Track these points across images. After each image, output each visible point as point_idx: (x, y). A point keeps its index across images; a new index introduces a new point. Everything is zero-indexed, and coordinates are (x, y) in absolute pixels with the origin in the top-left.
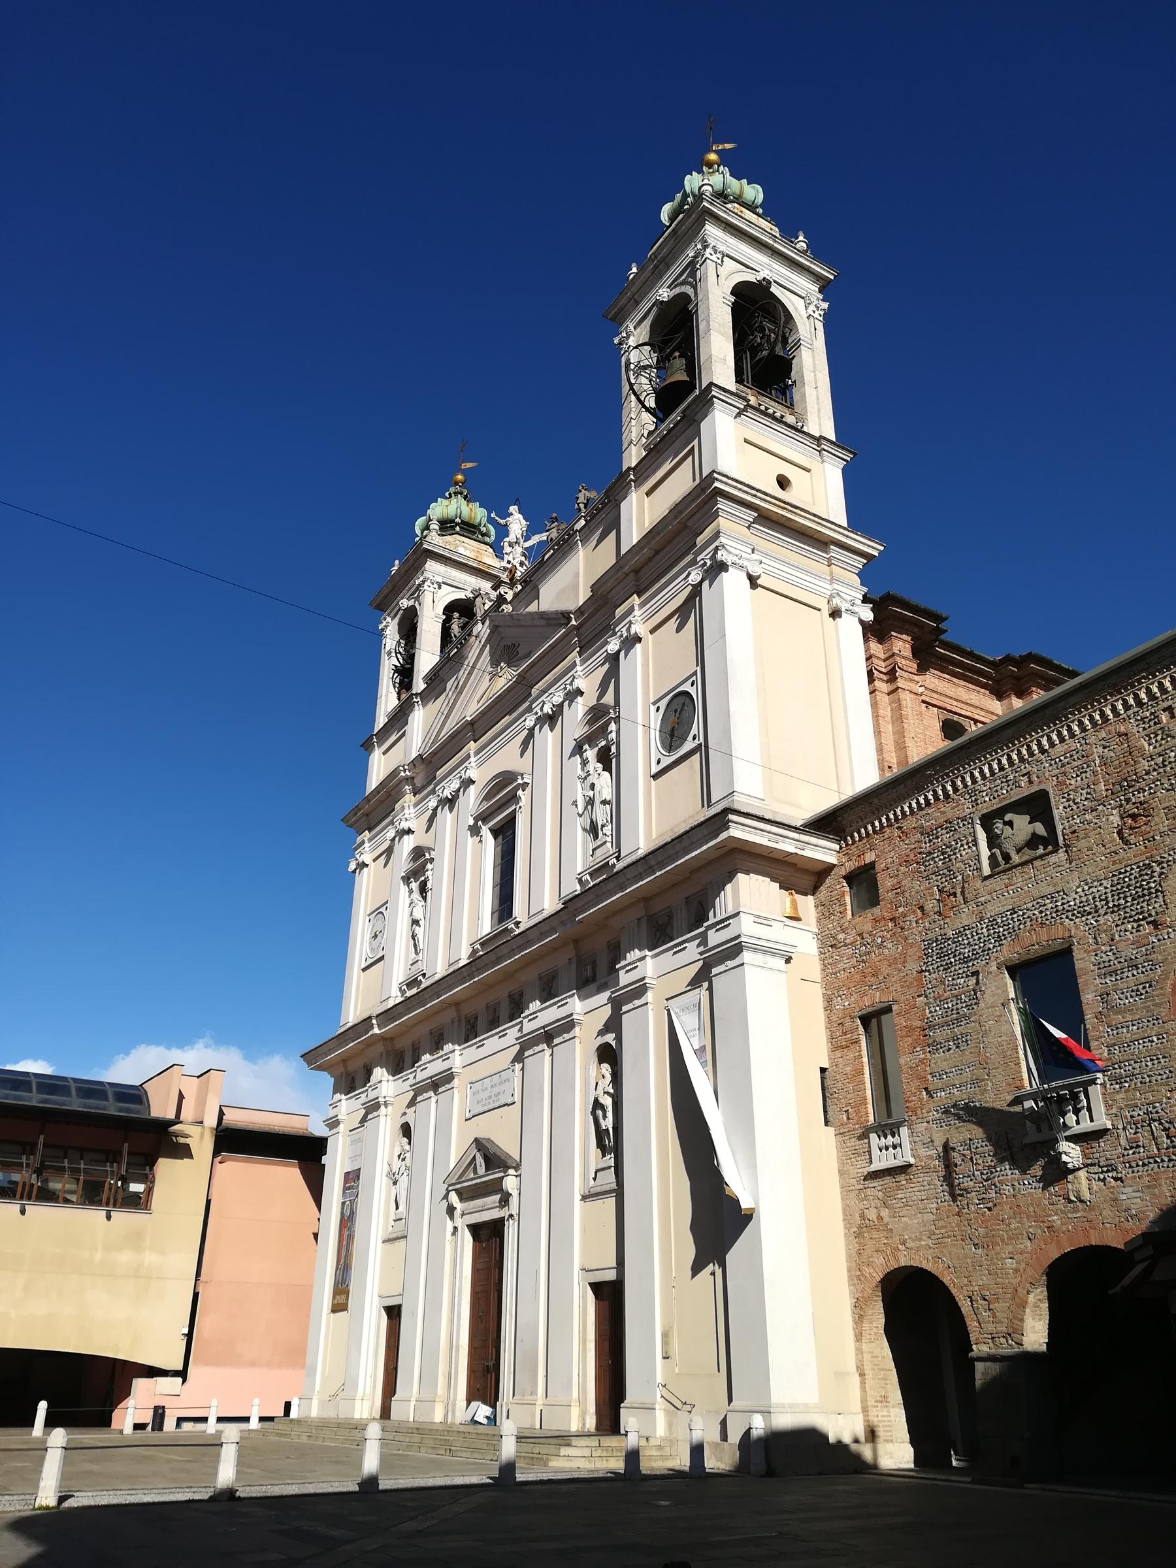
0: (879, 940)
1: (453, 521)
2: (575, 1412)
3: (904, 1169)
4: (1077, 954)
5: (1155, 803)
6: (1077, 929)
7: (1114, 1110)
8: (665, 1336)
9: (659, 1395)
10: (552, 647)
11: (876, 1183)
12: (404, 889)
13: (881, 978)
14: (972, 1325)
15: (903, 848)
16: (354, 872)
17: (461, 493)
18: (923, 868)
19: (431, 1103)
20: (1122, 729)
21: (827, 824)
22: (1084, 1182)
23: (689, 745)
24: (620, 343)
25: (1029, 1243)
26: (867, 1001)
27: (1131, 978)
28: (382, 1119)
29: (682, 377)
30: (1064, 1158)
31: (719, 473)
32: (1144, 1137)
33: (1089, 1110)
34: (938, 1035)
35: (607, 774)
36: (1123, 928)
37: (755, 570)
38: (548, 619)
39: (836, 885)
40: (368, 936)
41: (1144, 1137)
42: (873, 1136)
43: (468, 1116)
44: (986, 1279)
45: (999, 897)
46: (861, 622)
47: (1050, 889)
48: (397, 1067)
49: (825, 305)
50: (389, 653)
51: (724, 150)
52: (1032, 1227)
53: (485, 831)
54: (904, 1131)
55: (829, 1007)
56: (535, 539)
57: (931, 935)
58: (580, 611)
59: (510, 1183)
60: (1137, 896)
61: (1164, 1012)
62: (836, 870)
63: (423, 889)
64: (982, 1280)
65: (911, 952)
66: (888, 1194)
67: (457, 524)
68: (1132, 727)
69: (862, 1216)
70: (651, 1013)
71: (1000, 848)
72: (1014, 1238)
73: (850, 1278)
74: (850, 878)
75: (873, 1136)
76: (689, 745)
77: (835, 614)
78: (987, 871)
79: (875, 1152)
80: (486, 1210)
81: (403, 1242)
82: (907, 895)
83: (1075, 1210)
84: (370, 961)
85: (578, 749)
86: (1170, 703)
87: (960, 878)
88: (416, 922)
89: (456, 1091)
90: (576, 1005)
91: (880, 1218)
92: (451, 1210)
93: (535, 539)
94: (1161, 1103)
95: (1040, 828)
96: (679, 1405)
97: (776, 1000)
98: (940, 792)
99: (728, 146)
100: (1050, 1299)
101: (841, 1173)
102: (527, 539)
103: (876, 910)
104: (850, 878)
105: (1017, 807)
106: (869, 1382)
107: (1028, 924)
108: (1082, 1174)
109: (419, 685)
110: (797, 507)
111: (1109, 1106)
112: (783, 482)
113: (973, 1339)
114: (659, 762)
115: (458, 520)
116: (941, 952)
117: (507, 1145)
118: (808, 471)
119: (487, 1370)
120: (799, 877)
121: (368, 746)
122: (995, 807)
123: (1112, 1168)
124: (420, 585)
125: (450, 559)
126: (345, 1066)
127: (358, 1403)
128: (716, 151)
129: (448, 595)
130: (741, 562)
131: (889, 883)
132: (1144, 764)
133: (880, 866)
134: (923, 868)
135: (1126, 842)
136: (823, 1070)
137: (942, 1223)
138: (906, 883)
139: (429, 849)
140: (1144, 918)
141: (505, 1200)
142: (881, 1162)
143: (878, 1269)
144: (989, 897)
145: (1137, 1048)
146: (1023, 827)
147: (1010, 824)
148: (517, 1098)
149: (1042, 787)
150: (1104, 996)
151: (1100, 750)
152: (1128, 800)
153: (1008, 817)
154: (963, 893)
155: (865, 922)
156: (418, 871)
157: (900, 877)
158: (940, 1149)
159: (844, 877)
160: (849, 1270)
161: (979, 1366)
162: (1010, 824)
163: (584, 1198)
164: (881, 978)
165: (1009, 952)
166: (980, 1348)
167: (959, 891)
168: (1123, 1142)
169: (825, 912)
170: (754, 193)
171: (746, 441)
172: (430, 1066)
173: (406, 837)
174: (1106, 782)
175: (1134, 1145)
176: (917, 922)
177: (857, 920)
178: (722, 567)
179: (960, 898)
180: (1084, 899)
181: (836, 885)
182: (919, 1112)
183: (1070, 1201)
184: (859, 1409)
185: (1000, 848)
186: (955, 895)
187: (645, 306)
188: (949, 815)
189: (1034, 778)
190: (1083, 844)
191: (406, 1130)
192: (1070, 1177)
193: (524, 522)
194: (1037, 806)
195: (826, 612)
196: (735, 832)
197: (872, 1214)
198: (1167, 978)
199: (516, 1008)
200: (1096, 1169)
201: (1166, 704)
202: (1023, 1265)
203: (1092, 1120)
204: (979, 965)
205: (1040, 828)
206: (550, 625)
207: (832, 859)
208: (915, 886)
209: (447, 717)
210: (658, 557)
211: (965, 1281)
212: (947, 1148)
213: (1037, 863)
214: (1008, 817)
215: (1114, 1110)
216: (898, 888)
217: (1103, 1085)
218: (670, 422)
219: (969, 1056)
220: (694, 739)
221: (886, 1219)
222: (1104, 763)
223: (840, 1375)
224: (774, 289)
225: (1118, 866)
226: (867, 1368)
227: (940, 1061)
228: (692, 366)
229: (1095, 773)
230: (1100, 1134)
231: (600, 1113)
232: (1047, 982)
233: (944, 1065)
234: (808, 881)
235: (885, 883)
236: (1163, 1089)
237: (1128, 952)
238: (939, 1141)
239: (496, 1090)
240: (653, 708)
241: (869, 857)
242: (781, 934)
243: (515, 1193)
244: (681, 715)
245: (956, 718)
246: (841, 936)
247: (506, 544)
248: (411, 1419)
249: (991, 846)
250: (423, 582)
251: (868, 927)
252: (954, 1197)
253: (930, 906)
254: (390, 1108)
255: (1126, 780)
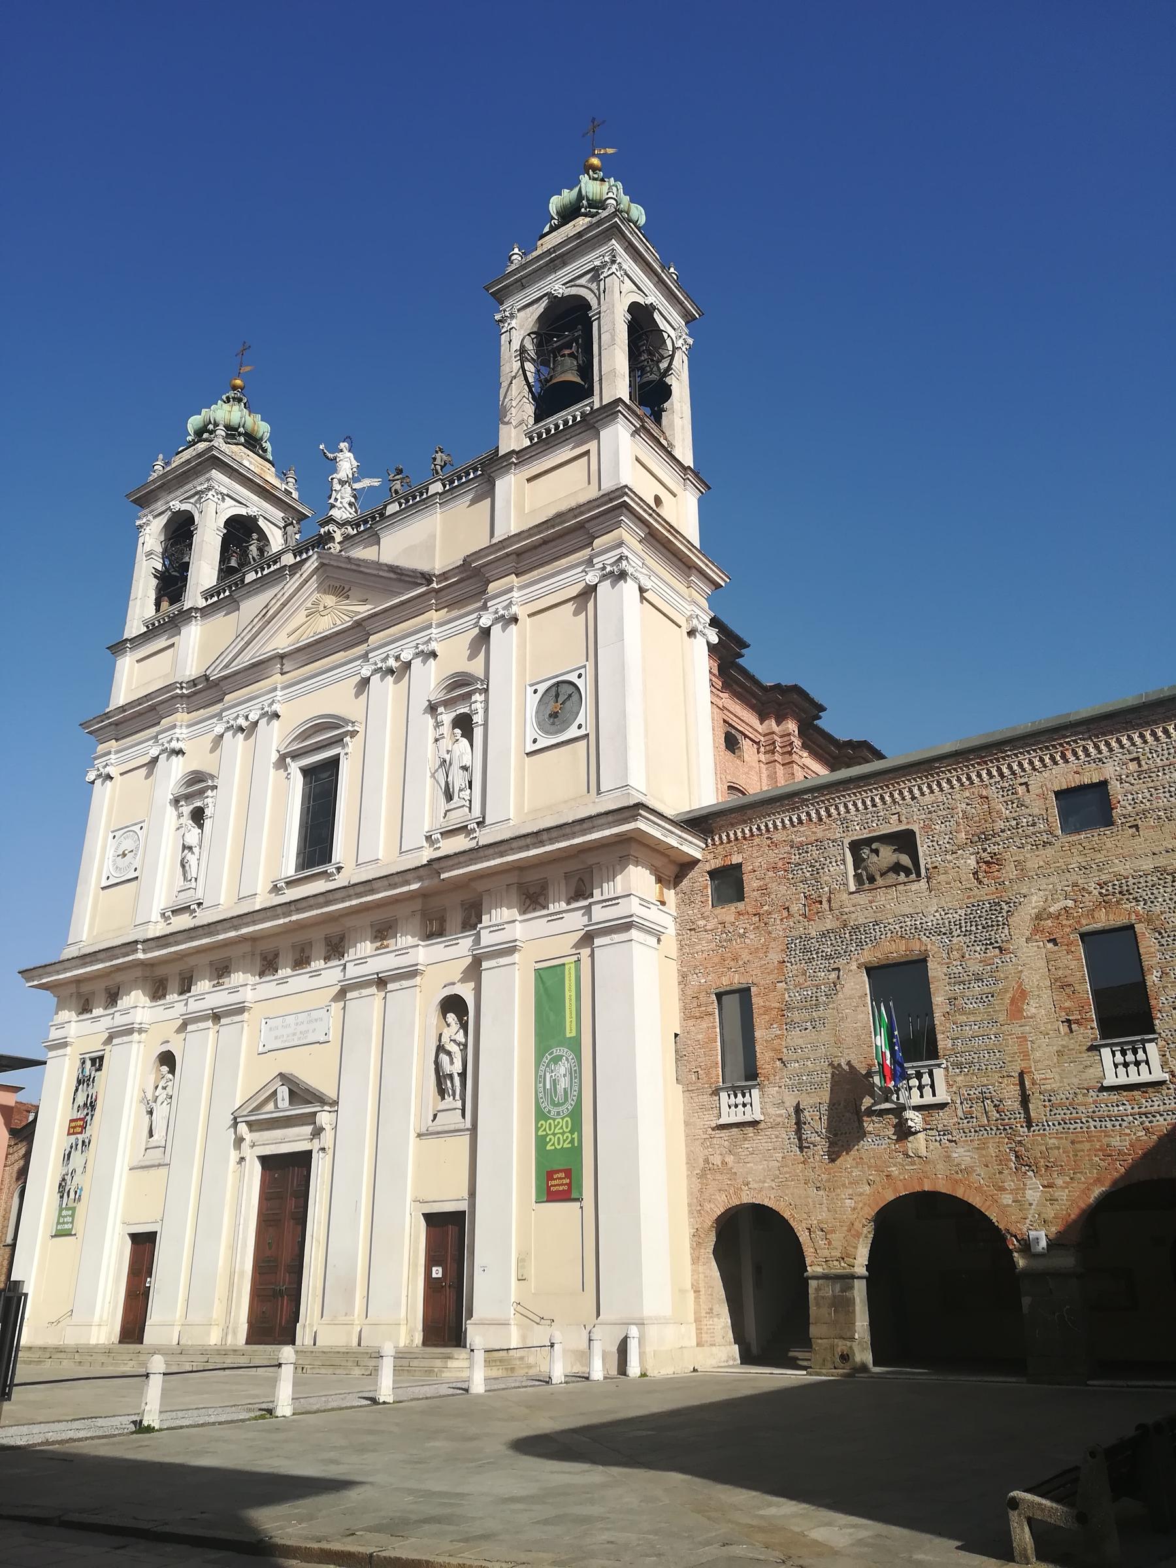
0: (742, 931)
1: (236, 430)
2: (403, 1330)
3: (754, 1123)
4: (931, 965)
5: (1007, 856)
6: (933, 945)
7: (954, 1089)
8: (521, 1261)
9: (513, 1312)
10: (403, 603)
11: (724, 1134)
12: (171, 811)
13: (741, 963)
14: (808, 1251)
15: (773, 856)
16: (93, 782)
17: (240, 400)
18: (791, 876)
19: (206, 1037)
20: (984, 793)
21: (700, 824)
22: (923, 1143)
23: (572, 732)
24: (502, 321)
25: (867, 1187)
26: (725, 981)
27: (977, 988)
28: (135, 1046)
29: (573, 377)
30: (910, 1123)
31: (630, 490)
32: (977, 1110)
33: (932, 1086)
34: (796, 1016)
35: (465, 741)
36: (973, 948)
37: (646, 583)
38: (402, 574)
39: (699, 879)
40: (110, 853)
41: (977, 1110)
42: (724, 1095)
43: (261, 1049)
44: (824, 1215)
45: (861, 907)
46: (708, 643)
47: (911, 911)
48: (158, 991)
49: (690, 341)
50: (149, 554)
51: (605, 154)
52: (873, 1175)
53: (294, 767)
54: (755, 1092)
55: (683, 978)
56: (366, 483)
57: (795, 933)
58: (444, 576)
59: (324, 1118)
60: (988, 922)
61: (1002, 1018)
62: (700, 865)
63: (198, 816)
64: (821, 1215)
65: (773, 944)
66: (734, 1142)
67: (240, 434)
68: (992, 792)
69: (707, 1161)
70: (517, 972)
71: (865, 869)
72: (855, 1183)
73: (691, 1212)
74: (713, 874)
75: (724, 1095)
76: (572, 732)
77: (691, 633)
78: (853, 888)
79: (724, 1107)
80: (291, 1141)
81: (163, 1171)
82: (773, 896)
83: (913, 1163)
84: (112, 881)
85: (432, 708)
86: (1026, 780)
87: (826, 889)
88: (187, 848)
89: (245, 1025)
90: (423, 953)
91: (724, 1163)
92: (239, 1141)
93: (366, 483)
94: (993, 1085)
95: (905, 860)
96: (538, 1320)
97: (647, 972)
98: (814, 815)
99: (610, 151)
100: (875, 1230)
101: (687, 1124)
102: (356, 480)
103: (741, 906)
104: (713, 874)
105: (886, 839)
106: (703, 1297)
107: (889, 935)
108: (921, 1136)
109: (193, 598)
110: (678, 532)
111: (949, 1085)
112: (658, 500)
113: (808, 1261)
114: (535, 741)
115: (241, 430)
116: (803, 948)
117: (317, 1079)
118: (675, 495)
119: (277, 1294)
120: (674, 871)
121: (118, 647)
122: (865, 836)
123: (946, 1132)
124: (202, 492)
125: (237, 471)
126: (78, 987)
127: (94, 1329)
128: (598, 156)
129: (231, 509)
130: (636, 574)
131: (756, 884)
132: (1000, 824)
133: (746, 868)
134: (791, 876)
135: (980, 882)
136: (676, 1035)
137: (786, 1169)
138: (773, 886)
139: (212, 777)
140: (991, 944)
141: (318, 1132)
142: (729, 1116)
143: (719, 1205)
144: (853, 909)
145: (976, 1042)
146: (888, 855)
147: (876, 852)
148: (334, 1036)
149: (909, 827)
150: (952, 1000)
151: (964, 806)
152: (985, 850)
153: (874, 846)
154: (829, 901)
155: (728, 913)
156: (195, 795)
157: (767, 880)
158: (792, 1110)
159: (709, 872)
160: (690, 1205)
161: (813, 1284)
162: (876, 852)
163: (419, 1135)
164: (741, 963)
165: (869, 955)
166: (814, 1268)
167: (824, 900)
168: (960, 1114)
169: (686, 901)
170: (638, 213)
171: (637, 460)
172: (206, 994)
173: (174, 758)
174: (967, 833)
175: (968, 1116)
176: (781, 920)
177: (718, 910)
178: (623, 575)
179: (825, 905)
180: (941, 922)
181: (699, 879)
182: (772, 1078)
183: (908, 1156)
184: (691, 1318)
185: (865, 869)
186: (821, 902)
187: (533, 292)
188: (820, 835)
189: (903, 818)
190: (942, 878)
191: (167, 1060)
192: (911, 1138)
193: (355, 464)
194: (905, 841)
195: (685, 630)
196: (641, 825)
197: (717, 1160)
198: (1006, 991)
199: (336, 949)
200: (934, 1133)
201: (1023, 780)
202: (861, 1205)
203: (934, 1095)
204: (840, 963)
205: (905, 860)
206: (400, 580)
207: (698, 855)
208: (780, 891)
209: (248, 644)
210: (544, 547)
211: (805, 1216)
212: (798, 1110)
213: (900, 888)
214: (874, 846)
215: (954, 1089)
216: (764, 889)
217: (946, 1069)
218: (550, 422)
219: (825, 1035)
220: (580, 727)
221: (730, 1165)
222: (965, 816)
223: (682, 1291)
224: (656, 316)
225: (972, 900)
226: (702, 1284)
227: (796, 1037)
228: (586, 370)
229: (958, 824)
230: (942, 1106)
231: (444, 1058)
232: (901, 986)
233: (800, 1042)
234: (671, 871)
235: (751, 883)
236: (996, 1076)
237: (975, 967)
238: (790, 1103)
239: (303, 1028)
240: (530, 690)
241: (736, 859)
242: (654, 915)
243: (328, 1127)
244: (560, 702)
245: (733, 732)
246: (701, 923)
247: (335, 481)
248: (175, 1342)
249: (856, 867)
250: (209, 489)
251: (730, 918)
252: (801, 1148)
253: (794, 909)
254: (144, 1035)
255: (983, 833)
